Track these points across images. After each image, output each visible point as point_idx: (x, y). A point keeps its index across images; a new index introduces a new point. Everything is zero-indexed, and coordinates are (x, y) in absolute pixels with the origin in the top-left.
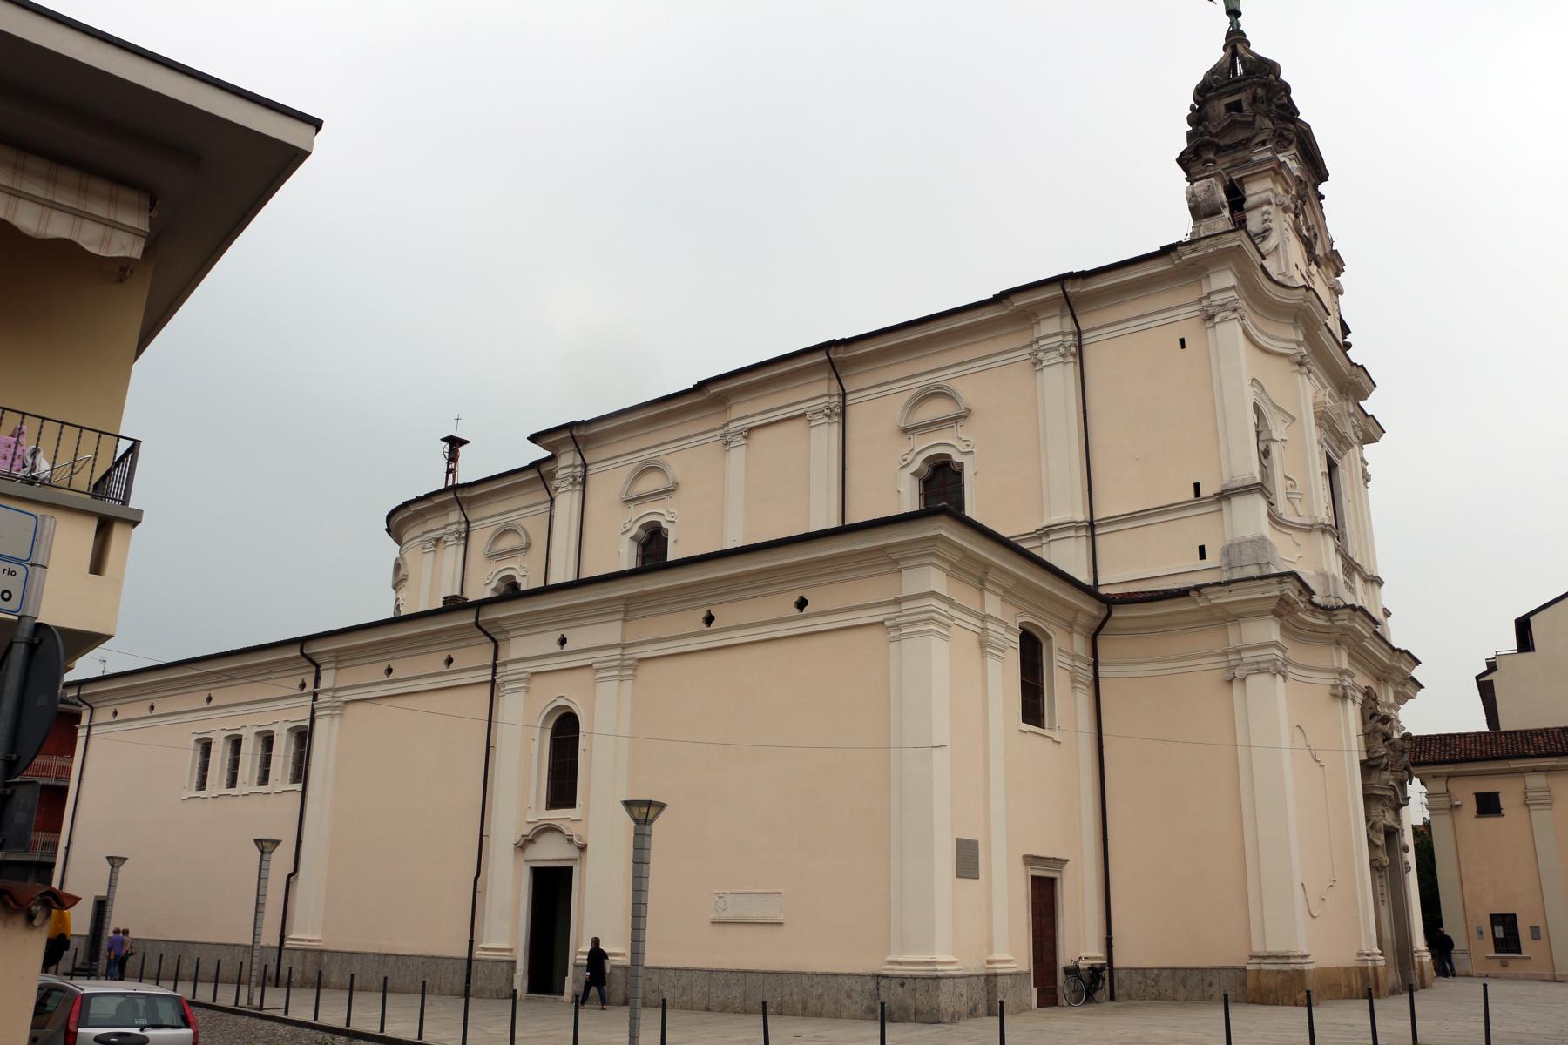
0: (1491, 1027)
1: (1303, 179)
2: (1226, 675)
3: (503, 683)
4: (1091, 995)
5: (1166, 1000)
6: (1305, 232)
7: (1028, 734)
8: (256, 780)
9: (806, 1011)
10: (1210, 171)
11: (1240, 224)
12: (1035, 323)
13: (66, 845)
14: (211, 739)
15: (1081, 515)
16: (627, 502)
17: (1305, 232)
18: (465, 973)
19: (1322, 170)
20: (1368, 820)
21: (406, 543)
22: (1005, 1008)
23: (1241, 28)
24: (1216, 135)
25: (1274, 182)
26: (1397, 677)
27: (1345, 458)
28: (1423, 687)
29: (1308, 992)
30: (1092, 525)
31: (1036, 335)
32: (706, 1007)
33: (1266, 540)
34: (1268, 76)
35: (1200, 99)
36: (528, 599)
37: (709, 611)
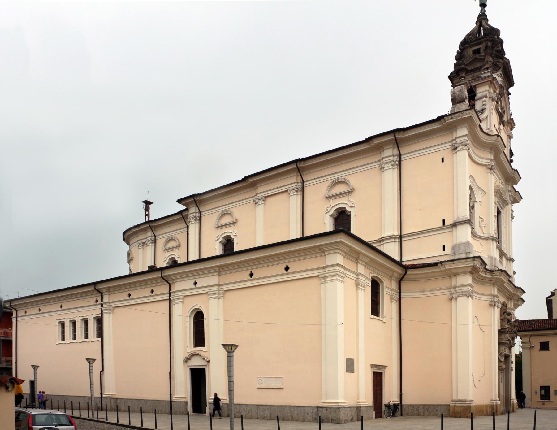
0: (536, 426)
1: (502, 85)
2: (450, 297)
3: (174, 300)
4: (394, 414)
5: (421, 416)
6: (500, 110)
7: (373, 319)
8: (83, 337)
9: (292, 419)
10: (462, 82)
11: (472, 107)
12: (382, 151)
13: (15, 361)
14: (76, 320)
15: (397, 233)
16: (217, 227)
17: (500, 110)
18: (170, 406)
19: (512, 81)
20: (499, 352)
21: (131, 245)
22: (363, 418)
23: (485, 13)
24: (467, 65)
25: (490, 87)
26: (516, 298)
27: (505, 209)
28: (525, 302)
29: (472, 413)
30: (401, 237)
31: (382, 156)
32: (257, 418)
33: (469, 243)
34: (494, 36)
35: (462, 48)
36: (193, 265)
37: (251, 272)
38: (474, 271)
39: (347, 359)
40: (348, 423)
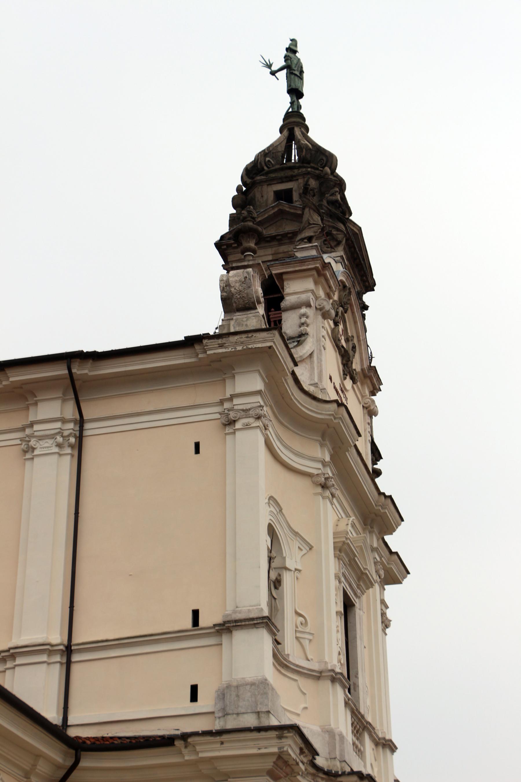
19: (370, 279)
25: (316, 283)
35: (249, 181)
38: (281, 769)
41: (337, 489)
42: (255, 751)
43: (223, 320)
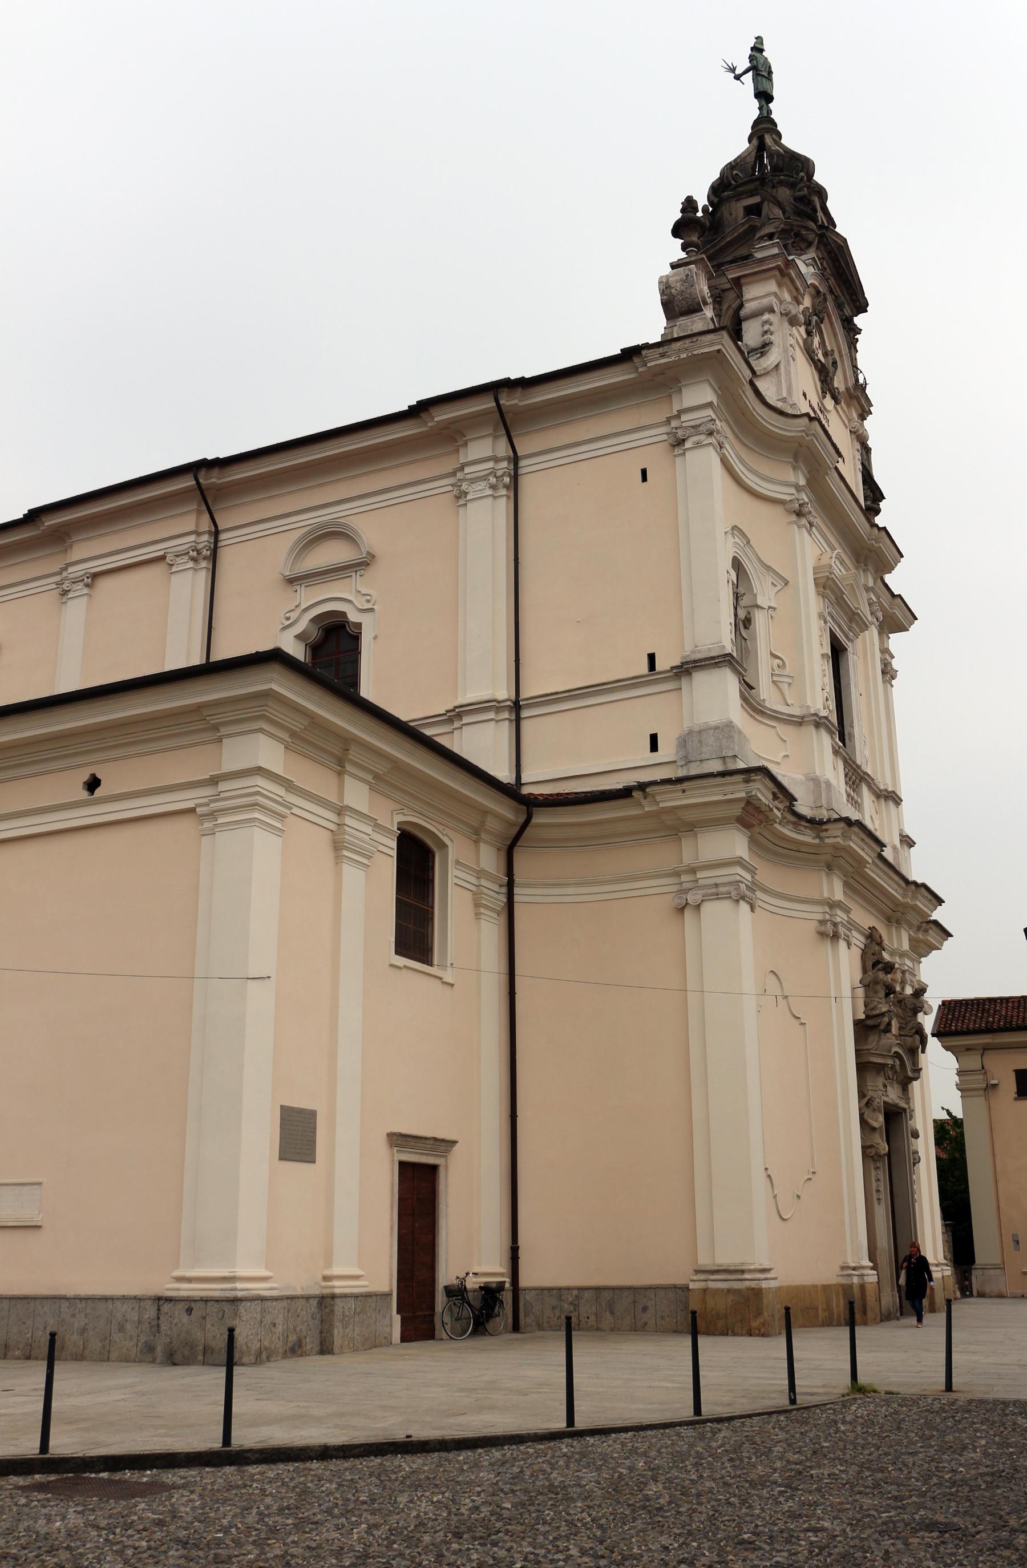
2: (677, 901)
4: (483, 1324)
7: (404, 971)
15: (504, 693)
19: (861, 299)
20: (862, 1095)
25: (779, 285)
30: (517, 706)
35: (716, 200)
38: (754, 816)
39: (286, 1111)
40: (269, 1364)
41: (816, 517)
42: (720, 798)
43: (665, 328)
